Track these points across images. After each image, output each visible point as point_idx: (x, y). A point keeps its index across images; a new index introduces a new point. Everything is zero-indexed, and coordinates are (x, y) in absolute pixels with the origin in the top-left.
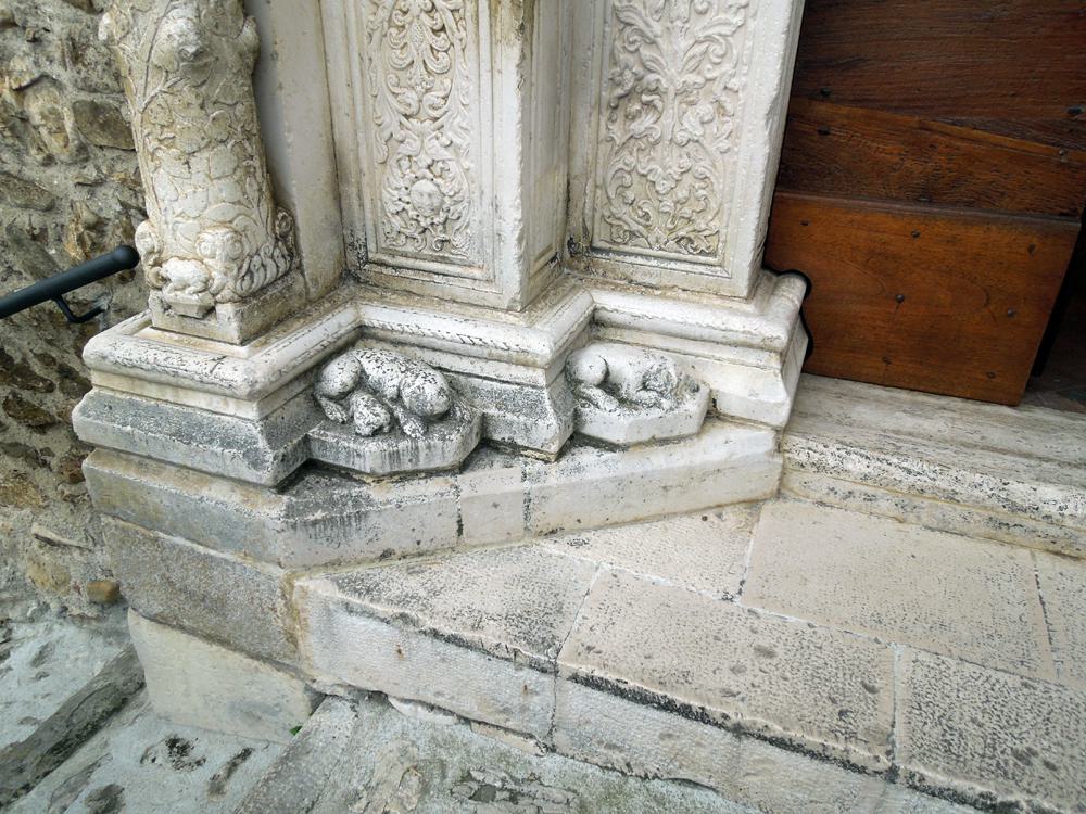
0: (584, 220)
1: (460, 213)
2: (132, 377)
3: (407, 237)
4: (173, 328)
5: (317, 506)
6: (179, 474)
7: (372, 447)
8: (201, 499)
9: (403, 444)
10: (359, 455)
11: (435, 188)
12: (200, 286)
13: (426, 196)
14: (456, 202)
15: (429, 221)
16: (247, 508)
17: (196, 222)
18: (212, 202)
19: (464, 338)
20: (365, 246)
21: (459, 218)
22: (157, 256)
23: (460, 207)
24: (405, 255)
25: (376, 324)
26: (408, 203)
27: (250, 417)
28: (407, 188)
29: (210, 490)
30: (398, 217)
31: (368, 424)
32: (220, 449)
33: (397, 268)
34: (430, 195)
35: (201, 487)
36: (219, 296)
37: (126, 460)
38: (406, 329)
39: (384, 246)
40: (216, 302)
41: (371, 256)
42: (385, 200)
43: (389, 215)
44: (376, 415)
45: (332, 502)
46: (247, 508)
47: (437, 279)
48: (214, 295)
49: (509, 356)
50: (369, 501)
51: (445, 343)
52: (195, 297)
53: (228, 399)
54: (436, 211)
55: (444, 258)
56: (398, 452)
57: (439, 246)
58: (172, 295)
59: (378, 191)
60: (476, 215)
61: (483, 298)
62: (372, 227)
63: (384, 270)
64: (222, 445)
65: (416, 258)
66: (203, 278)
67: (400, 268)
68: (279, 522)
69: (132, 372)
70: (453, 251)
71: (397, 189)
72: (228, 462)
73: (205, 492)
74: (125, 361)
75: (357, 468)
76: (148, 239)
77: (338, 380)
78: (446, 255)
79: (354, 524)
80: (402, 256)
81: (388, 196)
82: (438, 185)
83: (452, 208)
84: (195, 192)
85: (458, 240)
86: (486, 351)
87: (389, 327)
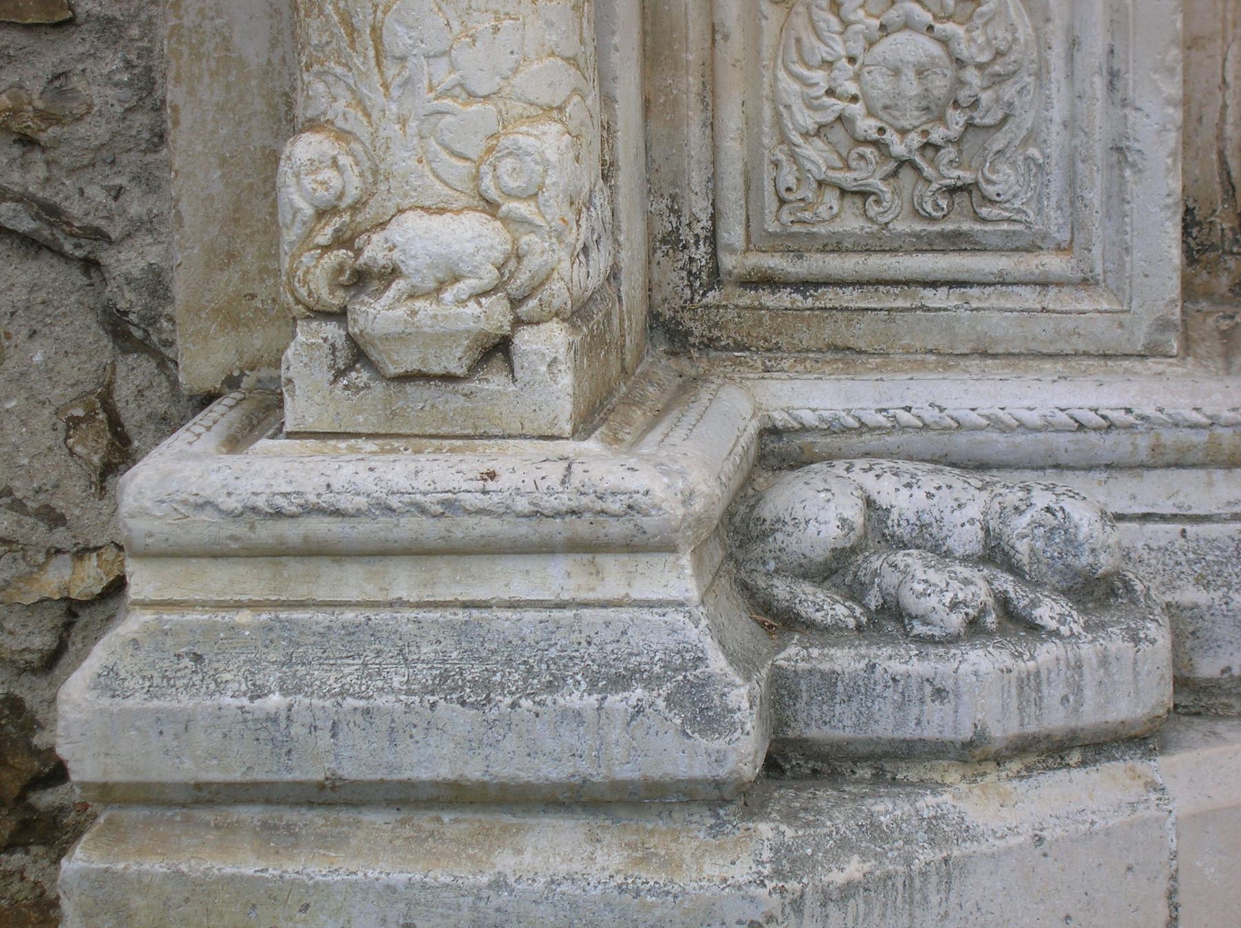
0: (1221, 154)
1: (1010, 104)
2: (278, 553)
3: (843, 192)
4: (362, 423)
5: (845, 845)
6: (408, 831)
7: (982, 661)
8: (498, 884)
9: (1047, 652)
10: (939, 693)
11: (935, 49)
12: (489, 276)
13: (910, 74)
14: (998, 80)
15: (915, 140)
16: (652, 876)
17: (490, 107)
18: (532, 56)
19: (1078, 414)
20: (713, 238)
21: (1005, 120)
22: (346, 218)
23: (1009, 91)
24: (836, 246)
25: (810, 419)
26: (854, 99)
27: (674, 594)
28: (852, 60)
29: (519, 852)
30: (819, 143)
31: (954, 605)
32: (593, 700)
33: (804, 285)
34: (921, 72)
35: (489, 853)
36: (532, 303)
37: (217, 827)
38: (905, 417)
39: (773, 227)
40: (518, 322)
41: (728, 262)
42: (785, 98)
43: (797, 139)
44: (966, 582)
45: (874, 830)
46: (652, 876)
47: (936, 298)
48: (515, 303)
49: (1215, 443)
50: (966, 833)
51: (1020, 438)
52: (472, 308)
53: (601, 559)
54: (934, 112)
55: (957, 235)
56: (1038, 674)
57: (944, 203)
58: (401, 312)
59: (767, 80)
60: (1050, 108)
61: (1075, 332)
62: (740, 180)
63: (768, 298)
64: (592, 687)
65: (869, 251)
66: (498, 256)
67: (817, 285)
68: (762, 892)
69: (292, 532)
70: (984, 211)
71: (828, 65)
72: (616, 733)
73: (505, 861)
74: (280, 501)
75: (930, 733)
76: (328, 174)
77: (831, 516)
78: (966, 226)
79: (934, 899)
80: (824, 250)
81: (796, 87)
82: (944, 42)
83: (986, 97)
84: (496, 30)
85: (1004, 180)
86: (1144, 442)
87: (851, 422)
